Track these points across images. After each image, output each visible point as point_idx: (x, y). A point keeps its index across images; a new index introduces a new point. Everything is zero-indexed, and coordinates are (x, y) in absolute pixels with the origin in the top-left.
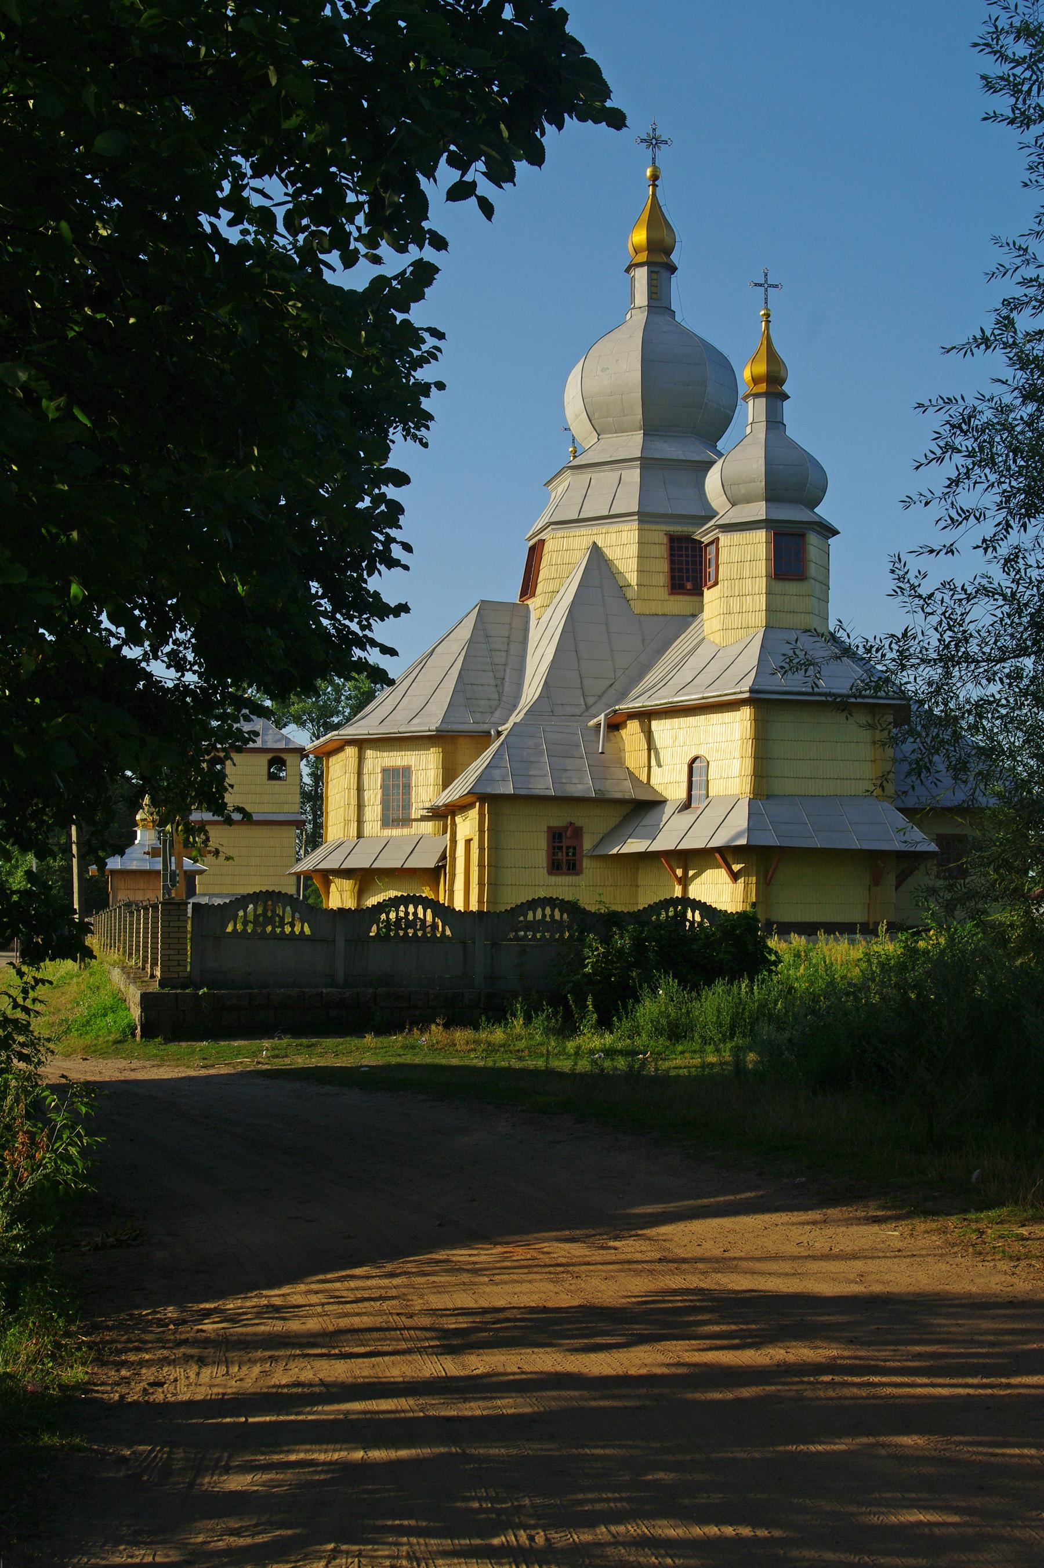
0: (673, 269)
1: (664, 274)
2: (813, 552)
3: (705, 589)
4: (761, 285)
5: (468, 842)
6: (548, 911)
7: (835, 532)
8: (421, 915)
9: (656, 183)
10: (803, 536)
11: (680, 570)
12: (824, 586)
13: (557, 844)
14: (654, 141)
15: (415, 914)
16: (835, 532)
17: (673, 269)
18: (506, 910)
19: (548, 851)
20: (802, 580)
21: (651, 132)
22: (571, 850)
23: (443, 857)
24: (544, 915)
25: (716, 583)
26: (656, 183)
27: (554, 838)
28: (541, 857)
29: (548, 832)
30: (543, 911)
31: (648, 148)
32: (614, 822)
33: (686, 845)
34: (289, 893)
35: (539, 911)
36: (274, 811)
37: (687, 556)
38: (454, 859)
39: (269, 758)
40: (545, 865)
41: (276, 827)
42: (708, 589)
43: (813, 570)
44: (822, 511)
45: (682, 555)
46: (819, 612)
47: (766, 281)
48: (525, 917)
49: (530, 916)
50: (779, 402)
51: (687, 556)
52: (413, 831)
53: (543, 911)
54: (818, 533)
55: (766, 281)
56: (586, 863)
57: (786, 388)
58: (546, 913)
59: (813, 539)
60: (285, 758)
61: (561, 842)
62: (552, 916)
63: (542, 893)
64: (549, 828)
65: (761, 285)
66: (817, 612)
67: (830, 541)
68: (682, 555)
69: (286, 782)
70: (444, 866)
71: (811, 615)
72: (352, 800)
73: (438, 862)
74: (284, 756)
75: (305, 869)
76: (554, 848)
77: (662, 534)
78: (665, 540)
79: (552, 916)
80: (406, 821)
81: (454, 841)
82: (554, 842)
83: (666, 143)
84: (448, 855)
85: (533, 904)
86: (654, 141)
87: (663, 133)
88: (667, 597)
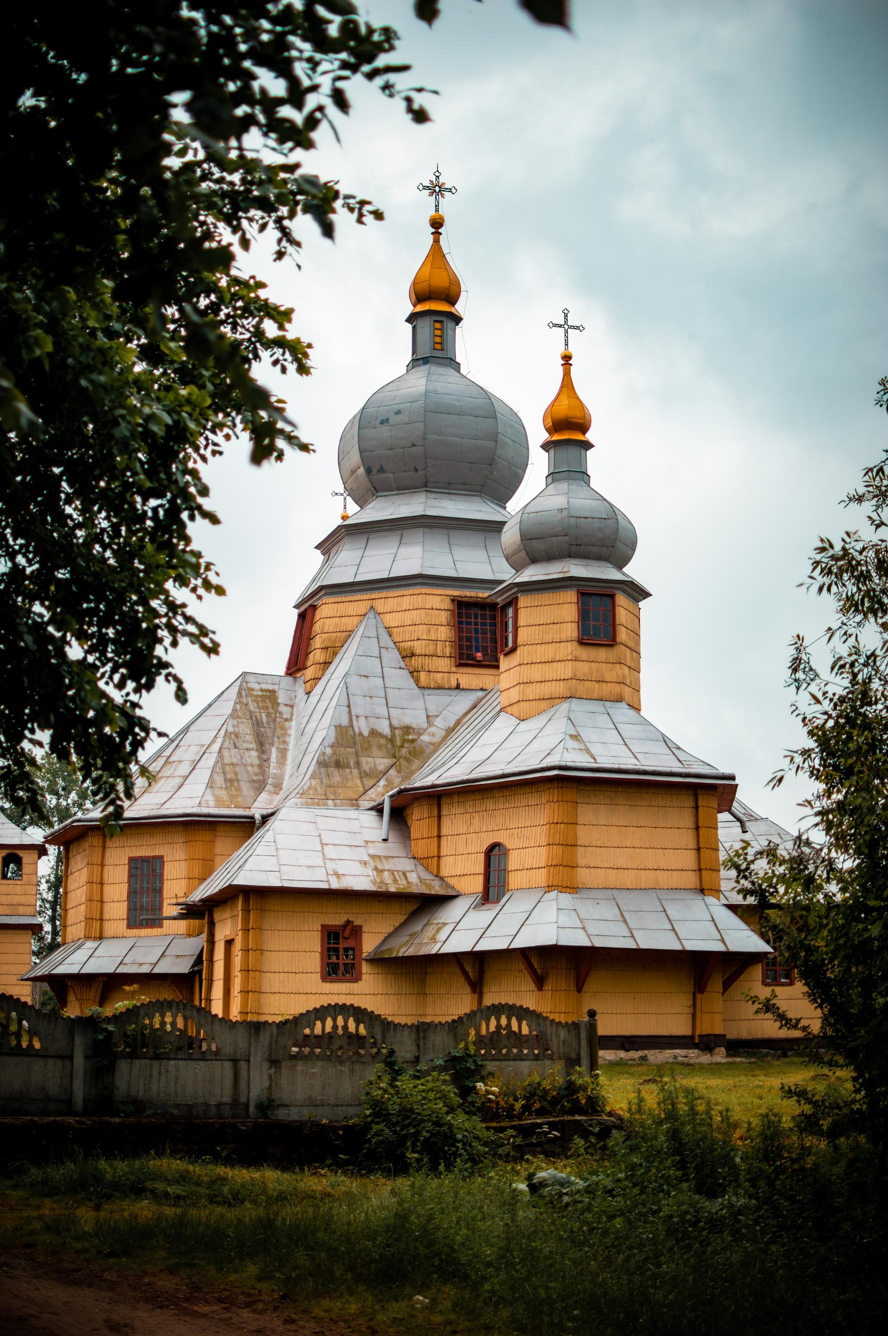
0: (457, 320)
1: (449, 324)
2: (622, 615)
3: (502, 657)
4: (560, 326)
5: (229, 943)
6: (340, 1021)
7: (646, 594)
8: (515, 1027)
9: (440, 230)
10: (612, 597)
11: (469, 639)
12: (635, 654)
13: (332, 945)
14: (437, 189)
15: (174, 1024)
16: (646, 594)
17: (457, 320)
18: (440, 1022)
19: (322, 953)
20: (611, 646)
21: (433, 179)
22: (351, 952)
23: (199, 961)
24: (335, 1027)
25: (514, 650)
26: (440, 230)
27: (329, 939)
28: (314, 961)
29: (322, 931)
30: (335, 1020)
31: (431, 194)
32: (402, 919)
33: (485, 946)
34: (23, 999)
35: (329, 1023)
36: (8, 913)
37: (476, 624)
38: (211, 961)
39: (4, 855)
40: (319, 969)
41: (10, 931)
42: (506, 655)
43: (622, 635)
44: (634, 571)
45: (476, 618)
46: (631, 682)
47: (566, 322)
48: (312, 1030)
49: (318, 1029)
50: (583, 451)
51: (476, 624)
52: (164, 930)
53: (335, 1020)
54: (629, 595)
55: (566, 322)
56: (365, 968)
57: (590, 436)
58: (338, 1024)
59: (621, 600)
60: (21, 855)
61: (338, 943)
62: (345, 1027)
63: (325, 1001)
64: (323, 926)
65: (560, 326)
66: (628, 683)
67: (641, 604)
68: (476, 618)
69: (22, 882)
70: (200, 972)
71: (622, 685)
72: (94, 895)
73: (193, 966)
74: (21, 853)
75: (40, 974)
76: (329, 949)
77: (448, 600)
78: (447, 604)
79: (345, 1027)
80: (155, 922)
81: (211, 942)
82: (329, 943)
83: (450, 190)
84: (204, 959)
85: (321, 1013)
86: (437, 189)
87: (447, 180)
88: (454, 669)
